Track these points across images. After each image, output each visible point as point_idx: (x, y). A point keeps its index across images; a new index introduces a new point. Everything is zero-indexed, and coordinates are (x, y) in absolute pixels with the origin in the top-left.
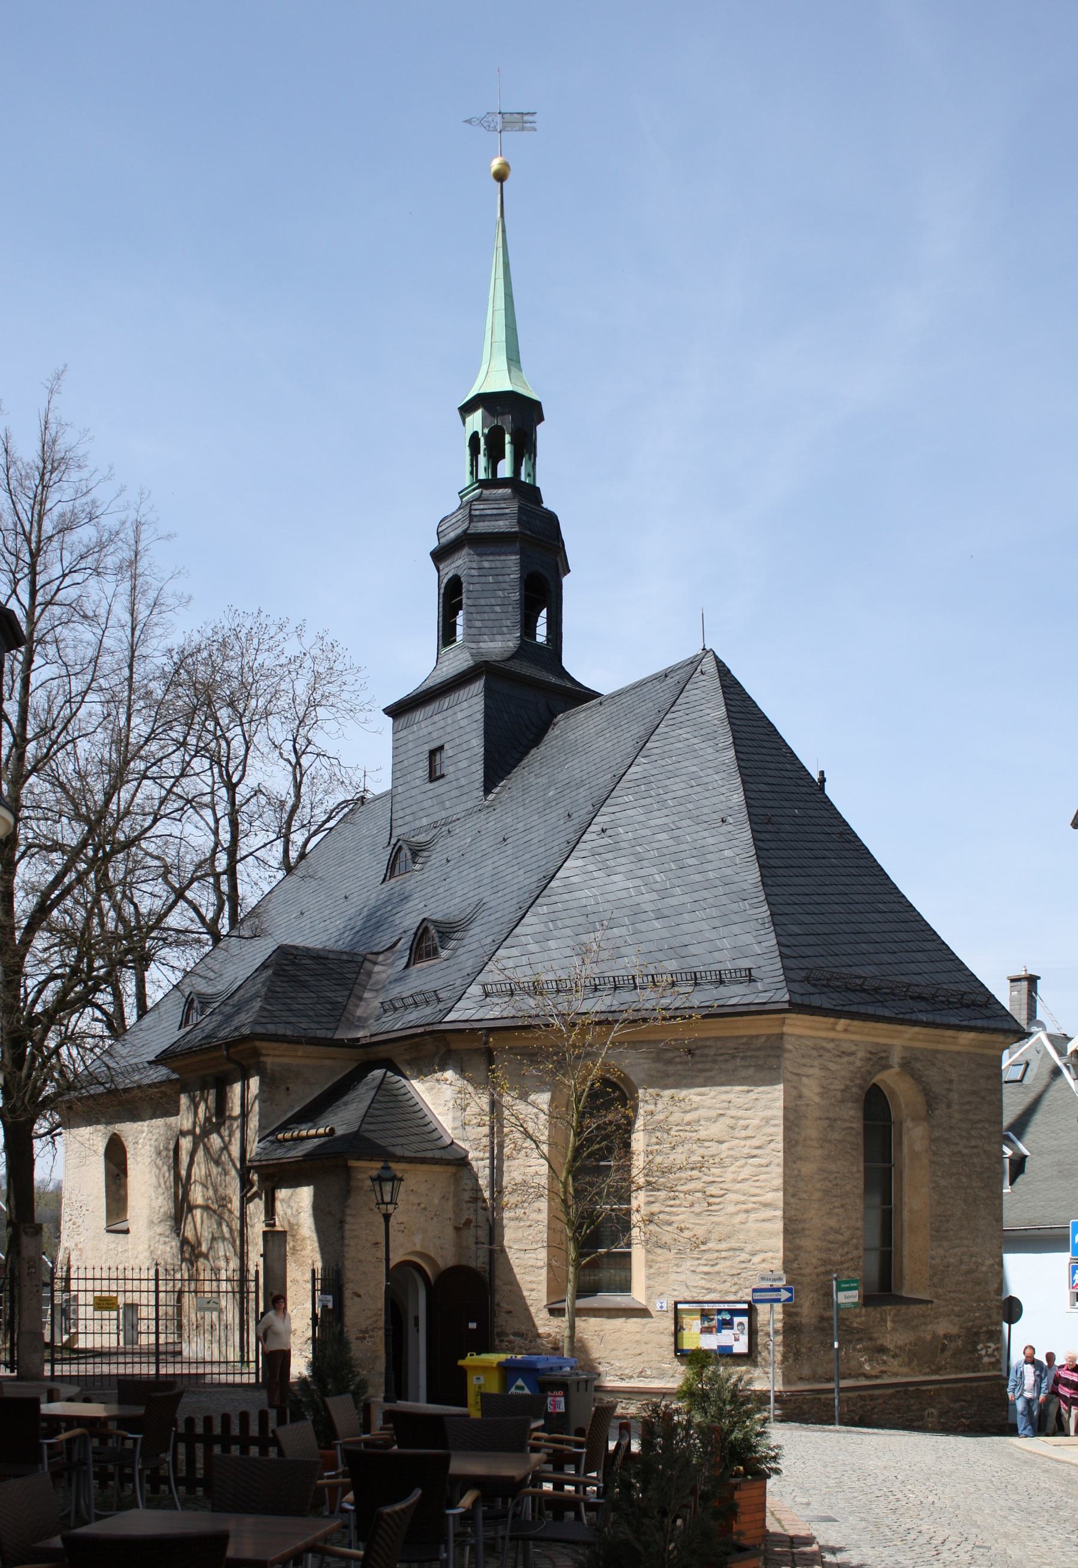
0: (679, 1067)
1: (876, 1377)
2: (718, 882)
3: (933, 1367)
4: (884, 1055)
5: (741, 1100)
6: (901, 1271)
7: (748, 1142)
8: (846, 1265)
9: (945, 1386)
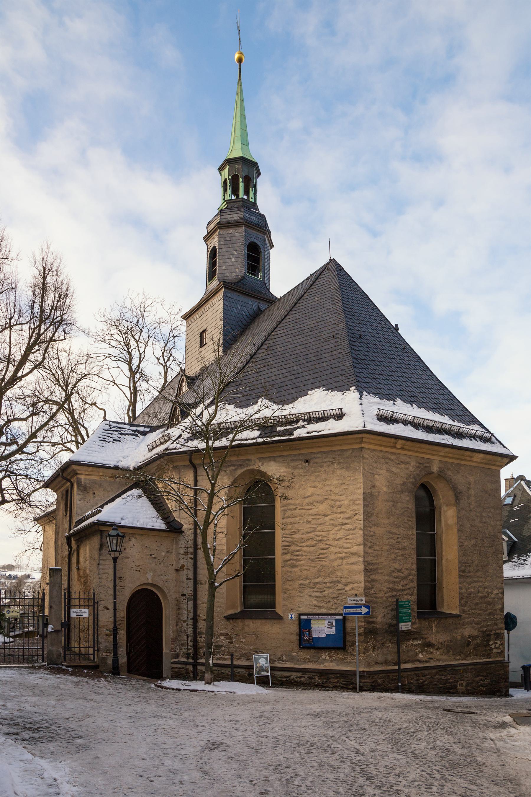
0: (301, 471)
1: (426, 662)
2: (328, 367)
3: (462, 655)
4: (427, 465)
5: (338, 489)
6: (442, 596)
7: (342, 516)
8: (406, 592)
9: (470, 667)
